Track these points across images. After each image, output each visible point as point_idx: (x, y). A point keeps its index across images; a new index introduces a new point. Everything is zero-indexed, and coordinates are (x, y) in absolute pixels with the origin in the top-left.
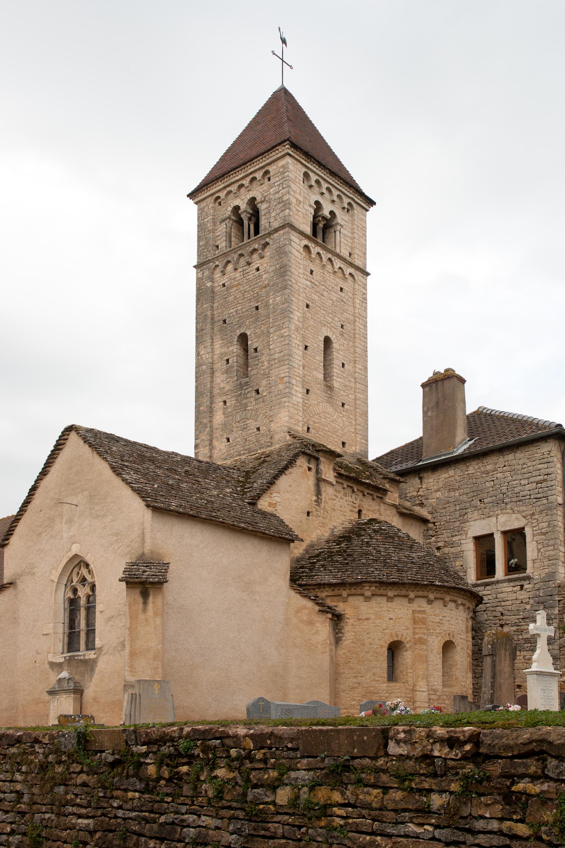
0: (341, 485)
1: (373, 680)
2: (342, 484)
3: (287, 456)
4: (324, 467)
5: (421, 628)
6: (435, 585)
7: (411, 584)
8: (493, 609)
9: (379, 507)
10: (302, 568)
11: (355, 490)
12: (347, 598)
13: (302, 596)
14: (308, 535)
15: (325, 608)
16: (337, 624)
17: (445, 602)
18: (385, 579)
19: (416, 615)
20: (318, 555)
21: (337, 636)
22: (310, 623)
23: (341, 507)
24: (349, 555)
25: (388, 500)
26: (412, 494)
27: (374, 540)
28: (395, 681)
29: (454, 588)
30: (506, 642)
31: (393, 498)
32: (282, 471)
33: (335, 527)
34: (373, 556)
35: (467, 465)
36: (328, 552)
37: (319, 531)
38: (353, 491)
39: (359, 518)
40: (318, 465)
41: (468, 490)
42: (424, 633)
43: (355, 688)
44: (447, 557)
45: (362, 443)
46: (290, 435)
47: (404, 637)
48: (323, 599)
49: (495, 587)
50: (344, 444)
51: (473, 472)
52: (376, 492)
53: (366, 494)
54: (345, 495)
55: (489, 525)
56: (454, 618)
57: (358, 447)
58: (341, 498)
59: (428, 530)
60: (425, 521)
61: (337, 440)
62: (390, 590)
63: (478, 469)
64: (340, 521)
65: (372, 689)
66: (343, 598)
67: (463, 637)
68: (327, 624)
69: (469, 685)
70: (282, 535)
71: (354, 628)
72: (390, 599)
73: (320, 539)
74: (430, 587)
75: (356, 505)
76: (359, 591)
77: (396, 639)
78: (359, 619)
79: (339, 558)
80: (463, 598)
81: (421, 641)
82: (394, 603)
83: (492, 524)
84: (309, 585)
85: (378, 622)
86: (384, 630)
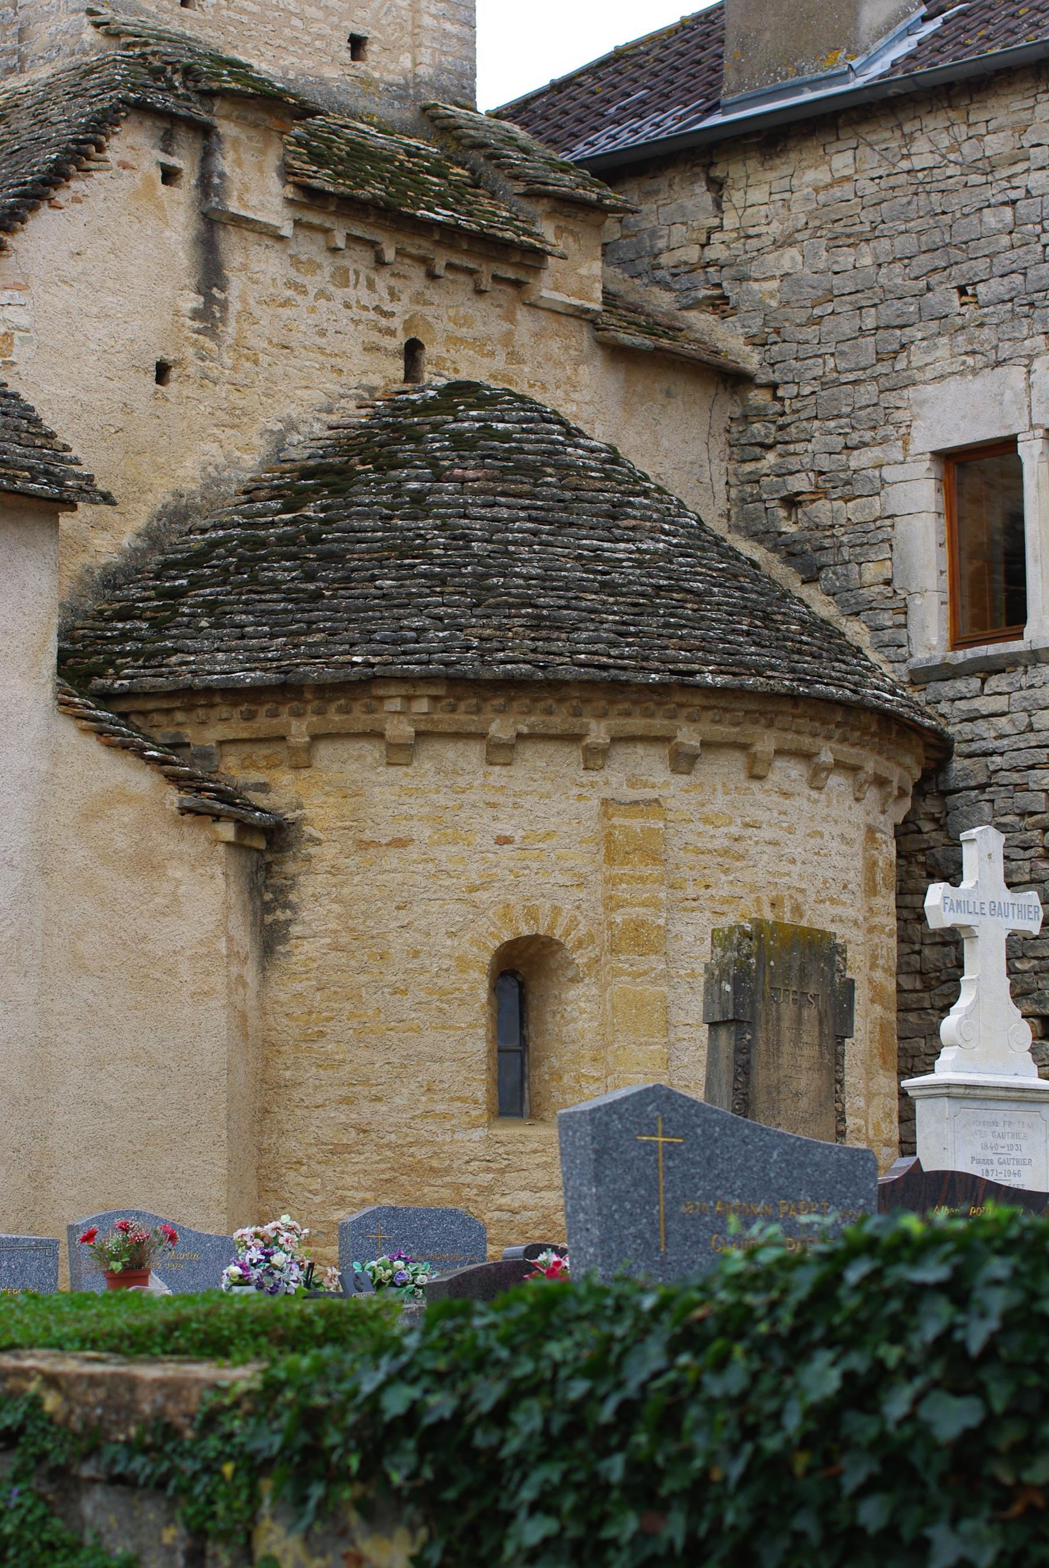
0: (320, 238)
1: (426, 1114)
2: (327, 231)
3: (67, 119)
4: (238, 162)
5: (642, 879)
6: (697, 687)
7: (591, 684)
8: (1016, 778)
9: (506, 326)
10: (123, 616)
11: (390, 255)
12: (309, 749)
13: (110, 745)
14: (159, 468)
15: (205, 799)
16: (269, 866)
17: (753, 760)
18: (469, 665)
19: (616, 821)
20: (198, 559)
21: (269, 919)
22: (146, 864)
23: (322, 333)
24: (329, 558)
25: (547, 289)
26: (681, 255)
27: (450, 487)
28: (532, 1116)
29: (793, 697)
30: (802, 969)
31: (573, 284)
32: (39, 192)
33: (292, 426)
34: (430, 559)
35: (907, 128)
36: (243, 542)
37: (212, 448)
38: (380, 262)
39: (406, 380)
40: (207, 156)
41: (905, 244)
42: (652, 903)
43: (347, 1149)
44: (827, 543)
45: (446, 35)
46: (97, 25)
47: (563, 922)
48: (205, 755)
49: (1024, 681)
50: (357, 44)
51: (928, 160)
52: (489, 258)
53: (439, 270)
54: (341, 278)
55: (998, 399)
56: (801, 831)
57: (425, 56)
58: (321, 294)
59: (746, 419)
60: (733, 380)
61: (328, 31)
62: (500, 711)
63: (951, 149)
64: (317, 397)
65: (421, 1153)
66: (294, 751)
67: (850, 912)
68: (218, 870)
69: (877, 1128)
70: (13, 479)
71: (343, 884)
72: (500, 753)
73: (217, 482)
74: (678, 698)
75: (396, 323)
76: (360, 719)
77: (525, 931)
78: (363, 845)
79: (283, 572)
80: (844, 740)
81: (641, 938)
82: (518, 771)
83: (1008, 395)
84: (147, 695)
85: (443, 854)
86: (473, 889)
